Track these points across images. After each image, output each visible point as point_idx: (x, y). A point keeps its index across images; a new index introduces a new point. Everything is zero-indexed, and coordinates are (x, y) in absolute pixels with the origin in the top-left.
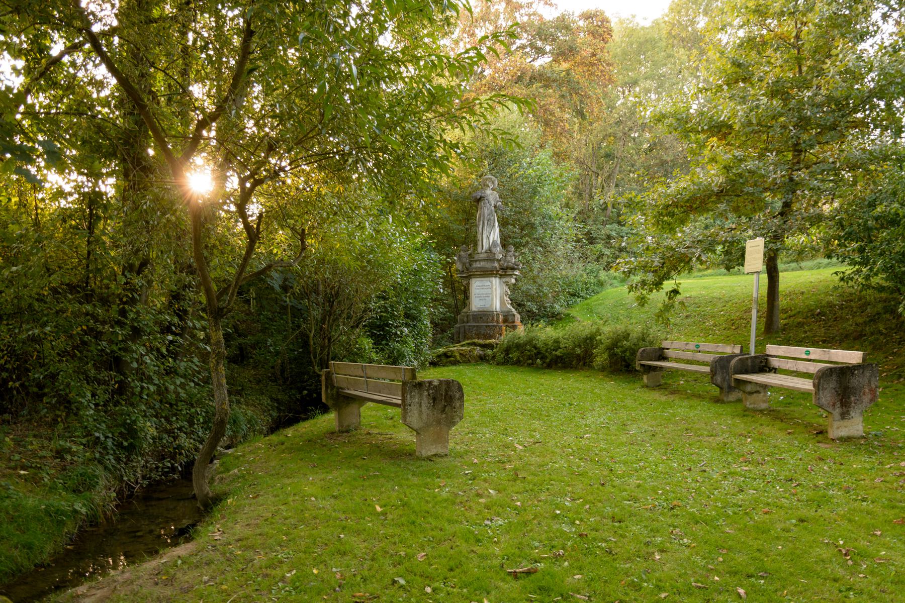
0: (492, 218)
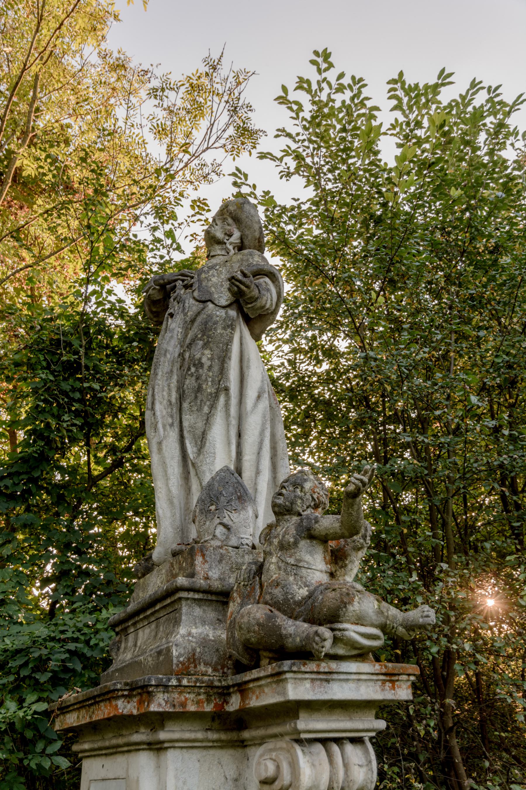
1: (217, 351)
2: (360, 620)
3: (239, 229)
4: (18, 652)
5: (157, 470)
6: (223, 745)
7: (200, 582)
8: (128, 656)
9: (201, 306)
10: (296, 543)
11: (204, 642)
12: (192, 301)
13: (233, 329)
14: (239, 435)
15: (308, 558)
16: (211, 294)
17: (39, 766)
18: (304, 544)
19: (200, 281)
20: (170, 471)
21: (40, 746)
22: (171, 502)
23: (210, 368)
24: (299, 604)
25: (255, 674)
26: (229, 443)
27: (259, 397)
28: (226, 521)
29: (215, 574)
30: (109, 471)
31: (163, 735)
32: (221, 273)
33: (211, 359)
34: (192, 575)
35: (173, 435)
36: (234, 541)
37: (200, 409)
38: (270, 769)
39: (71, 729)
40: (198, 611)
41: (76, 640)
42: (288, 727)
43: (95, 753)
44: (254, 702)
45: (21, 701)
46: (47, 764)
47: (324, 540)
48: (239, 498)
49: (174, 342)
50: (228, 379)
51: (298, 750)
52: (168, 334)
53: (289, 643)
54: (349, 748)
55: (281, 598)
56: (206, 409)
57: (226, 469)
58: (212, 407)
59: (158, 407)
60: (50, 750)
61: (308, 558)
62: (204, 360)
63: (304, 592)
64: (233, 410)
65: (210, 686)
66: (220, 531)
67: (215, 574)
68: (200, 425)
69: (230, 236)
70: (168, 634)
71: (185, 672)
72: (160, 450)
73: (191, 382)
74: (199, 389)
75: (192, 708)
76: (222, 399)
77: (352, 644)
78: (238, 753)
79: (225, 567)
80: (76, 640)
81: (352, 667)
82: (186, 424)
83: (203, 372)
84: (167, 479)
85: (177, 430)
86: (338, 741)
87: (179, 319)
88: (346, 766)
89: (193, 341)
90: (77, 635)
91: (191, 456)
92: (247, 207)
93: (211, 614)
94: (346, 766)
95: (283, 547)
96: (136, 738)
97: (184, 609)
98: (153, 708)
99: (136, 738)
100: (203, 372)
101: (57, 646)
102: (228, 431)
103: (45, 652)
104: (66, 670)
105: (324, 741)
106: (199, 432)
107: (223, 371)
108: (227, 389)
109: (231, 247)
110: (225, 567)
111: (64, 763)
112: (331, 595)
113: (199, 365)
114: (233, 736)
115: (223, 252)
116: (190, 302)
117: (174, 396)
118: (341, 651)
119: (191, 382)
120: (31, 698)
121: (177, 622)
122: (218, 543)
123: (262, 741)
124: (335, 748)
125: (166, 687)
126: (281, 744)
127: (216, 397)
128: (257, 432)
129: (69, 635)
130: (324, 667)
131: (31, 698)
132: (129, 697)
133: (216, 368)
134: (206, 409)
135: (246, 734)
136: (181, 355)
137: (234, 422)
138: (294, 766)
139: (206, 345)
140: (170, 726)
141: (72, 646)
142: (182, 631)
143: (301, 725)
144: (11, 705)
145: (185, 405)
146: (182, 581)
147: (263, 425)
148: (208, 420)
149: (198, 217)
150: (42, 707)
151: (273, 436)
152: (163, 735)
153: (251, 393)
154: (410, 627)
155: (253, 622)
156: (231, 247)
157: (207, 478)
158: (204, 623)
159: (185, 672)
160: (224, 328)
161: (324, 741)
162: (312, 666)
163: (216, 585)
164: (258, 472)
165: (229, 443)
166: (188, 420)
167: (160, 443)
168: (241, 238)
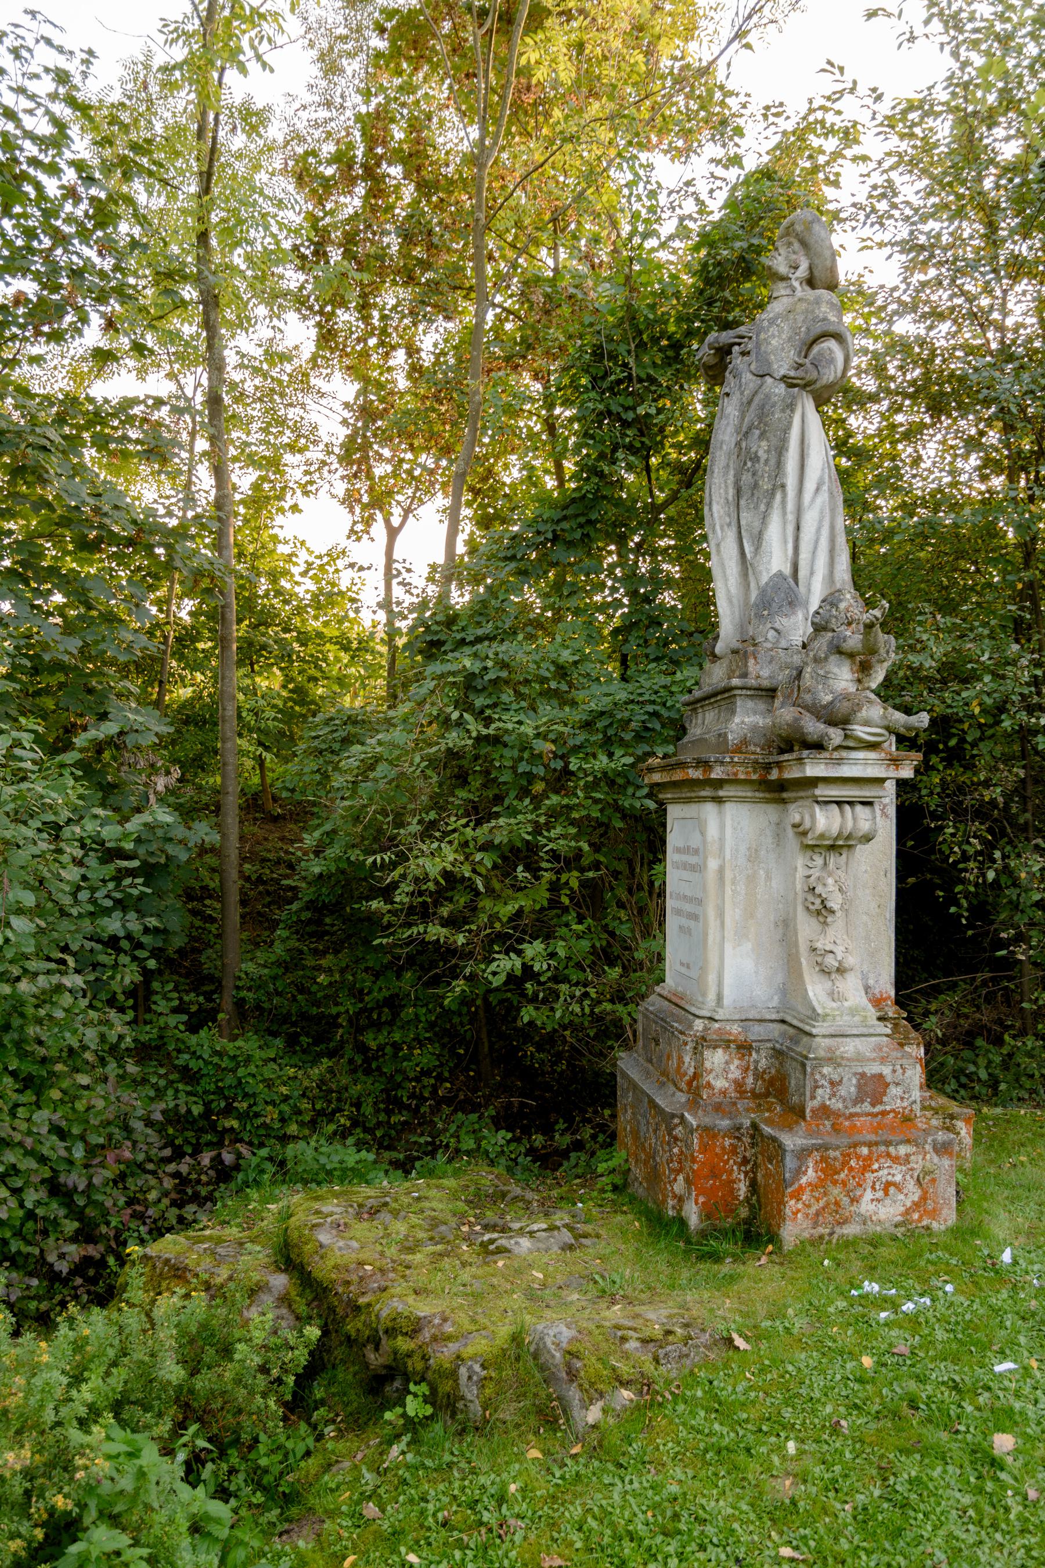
0: (762, 449)
1: (774, 441)
2: (867, 723)
3: (807, 255)
4: (602, 713)
5: (716, 573)
6: (768, 801)
7: (752, 682)
8: (699, 731)
9: (759, 381)
10: (826, 658)
11: (754, 728)
12: (749, 376)
13: (793, 411)
14: (798, 528)
15: (836, 670)
16: (769, 364)
17: (632, 806)
18: (834, 658)
19: (758, 345)
20: (728, 572)
21: (630, 790)
22: (730, 601)
23: (767, 461)
24: (825, 707)
25: (786, 757)
26: (785, 542)
27: (818, 490)
28: (777, 625)
29: (765, 673)
30: (674, 498)
31: (721, 793)
32: (782, 332)
33: (768, 451)
34: (744, 675)
35: (731, 535)
36: (783, 644)
37: (756, 508)
38: (797, 818)
39: (658, 784)
40: (750, 704)
41: (653, 702)
42: (809, 793)
43: (675, 801)
44: (788, 775)
45: (610, 755)
46: (638, 805)
47: (851, 656)
48: (790, 603)
49: (730, 429)
50: (784, 475)
51: (817, 808)
52: (724, 422)
53: (809, 738)
54: (859, 808)
55: (810, 702)
56: (762, 507)
57: (780, 574)
58: (769, 505)
59: (715, 508)
60: (638, 794)
61: (836, 670)
62: (761, 453)
63: (829, 698)
64: (790, 506)
65: (756, 762)
66: (771, 634)
67: (765, 673)
68: (757, 524)
69: (796, 268)
70: (728, 721)
71: (738, 750)
72: (718, 551)
73: (747, 478)
74: (756, 486)
75: (742, 777)
76: (778, 496)
77: (860, 740)
78: (781, 806)
79: (774, 666)
80: (653, 702)
81: (861, 755)
82: (743, 522)
83: (759, 467)
84: (726, 580)
85: (734, 529)
86: (849, 803)
87: (735, 399)
88: (854, 819)
89: (750, 429)
90: (654, 697)
91: (748, 556)
92: (816, 227)
93: (762, 706)
94: (854, 819)
95: (817, 660)
96: (703, 793)
97: (739, 703)
98: (713, 776)
99: (703, 793)
100: (759, 467)
101: (636, 707)
102: (784, 529)
103: (626, 714)
104: (647, 729)
105: (838, 803)
106: (756, 531)
107: (779, 465)
108: (783, 486)
109: (796, 284)
110: (774, 666)
111: (652, 805)
112: (846, 704)
113: (756, 459)
114: (776, 795)
115: (788, 292)
116: (747, 377)
117: (731, 492)
118: (851, 744)
119: (747, 478)
120: (619, 752)
121: (733, 712)
122: (769, 645)
123: (796, 800)
124: (847, 808)
125: (722, 763)
126: (807, 803)
127: (772, 494)
128: (813, 529)
129: (646, 697)
130: (836, 755)
131: (619, 752)
132: (696, 767)
133: (773, 462)
134: (762, 507)
135: (785, 795)
136: (738, 444)
137: (791, 517)
138: (813, 817)
139: (762, 436)
140: (727, 787)
141: (650, 708)
142: (737, 720)
143: (818, 792)
144: (604, 759)
145: (742, 502)
146: (736, 682)
147: (821, 521)
148: (765, 519)
149: (773, 128)
150: (629, 760)
151: (832, 528)
152: (721, 793)
153: (810, 486)
154: (909, 729)
155: (204, 1219)
156: (796, 284)
157: (764, 579)
158: (755, 713)
159: (738, 750)
160: (783, 411)
161: (838, 803)
162: (826, 755)
163: (766, 683)
164: (812, 573)
165: (785, 542)
166: (746, 517)
167: (718, 545)
168: (810, 268)
